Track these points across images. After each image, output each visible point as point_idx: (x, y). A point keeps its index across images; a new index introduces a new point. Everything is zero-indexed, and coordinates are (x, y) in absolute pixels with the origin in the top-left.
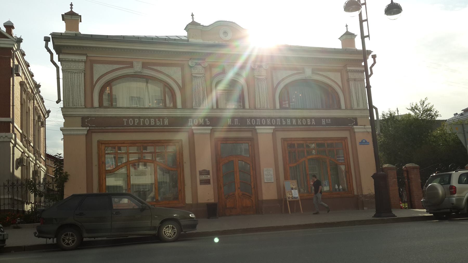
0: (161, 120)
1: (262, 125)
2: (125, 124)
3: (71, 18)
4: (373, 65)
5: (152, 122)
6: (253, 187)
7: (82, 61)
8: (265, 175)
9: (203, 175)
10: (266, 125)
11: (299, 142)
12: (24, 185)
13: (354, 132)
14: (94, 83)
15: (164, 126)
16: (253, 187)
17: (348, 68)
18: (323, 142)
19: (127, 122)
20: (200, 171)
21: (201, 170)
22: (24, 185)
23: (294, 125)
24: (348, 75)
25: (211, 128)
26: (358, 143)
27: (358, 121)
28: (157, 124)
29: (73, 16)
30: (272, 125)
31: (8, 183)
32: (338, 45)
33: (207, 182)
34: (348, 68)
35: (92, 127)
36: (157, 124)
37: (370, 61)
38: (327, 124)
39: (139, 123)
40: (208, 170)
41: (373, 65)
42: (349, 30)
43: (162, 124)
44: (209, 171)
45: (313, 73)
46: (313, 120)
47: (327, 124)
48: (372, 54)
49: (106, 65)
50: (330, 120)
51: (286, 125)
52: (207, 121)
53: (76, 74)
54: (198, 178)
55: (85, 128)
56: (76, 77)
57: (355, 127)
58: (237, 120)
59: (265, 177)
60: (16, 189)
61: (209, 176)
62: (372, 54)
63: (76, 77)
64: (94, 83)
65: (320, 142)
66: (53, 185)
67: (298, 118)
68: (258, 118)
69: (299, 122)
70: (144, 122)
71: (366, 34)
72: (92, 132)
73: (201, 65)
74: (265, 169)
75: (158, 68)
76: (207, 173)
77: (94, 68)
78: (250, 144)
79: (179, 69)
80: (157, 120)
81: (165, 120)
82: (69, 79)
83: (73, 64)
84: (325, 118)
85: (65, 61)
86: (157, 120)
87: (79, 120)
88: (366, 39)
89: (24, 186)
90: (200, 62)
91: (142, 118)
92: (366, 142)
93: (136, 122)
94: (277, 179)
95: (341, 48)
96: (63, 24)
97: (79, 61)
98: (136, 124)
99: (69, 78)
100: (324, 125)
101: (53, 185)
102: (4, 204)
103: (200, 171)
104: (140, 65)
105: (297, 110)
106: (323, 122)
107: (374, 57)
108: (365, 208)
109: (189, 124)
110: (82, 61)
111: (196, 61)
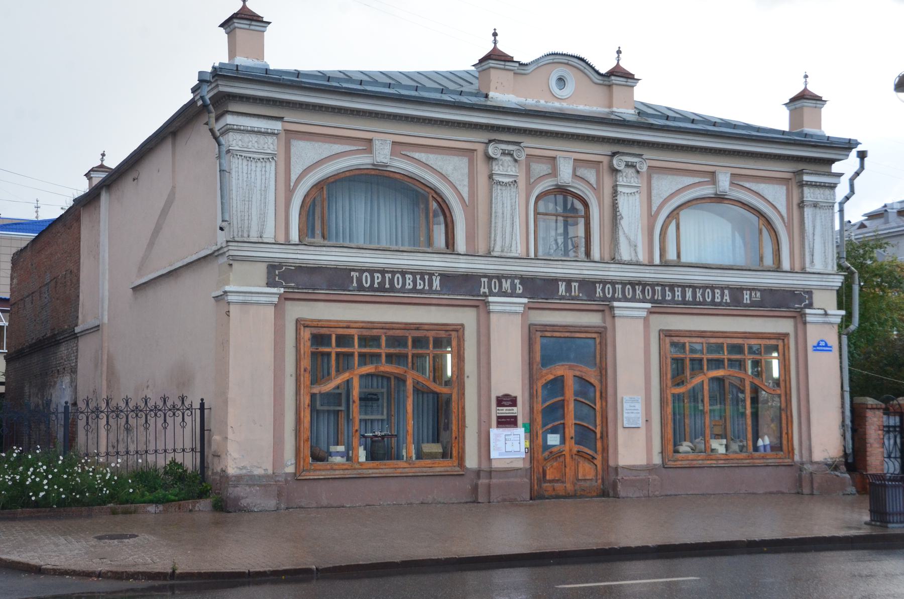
0: (427, 277)
1: (626, 300)
2: (355, 284)
3: (804, 101)
4: (857, 174)
5: (408, 281)
6: (598, 435)
13: (489, 312)
14: (292, 184)
15: (431, 291)
16: (598, 435)
17: (806, 178)
18: (740, 341)
19: (359, 280)
20: (498, 398)
21: (500, 394)
22: (121, 411)
25: (525, 300)
27: (814, 296)
28: (418, 287)
30: (644, 301)
33: (508, 422)
34: (806, 178)
35: (289, 288)
37: (846, 166)
40: (513, 395)
41: (857, 174)
42: (500, 47)
43: (427, 287)
44: (516, 397)
46: (726, 292)
47: (753, 304)
48: (860, 148)
50: (758, 294)
51: (403, 289)
52: (518, 286)
54: (496, 412)
55: (275, 290)
56: (258, 169)
57: (808, 311)
58: (577, 284)
59: (625, 415)
60: (104, 421)
61: (515, 408)
63: (258, 169)
64: (292, 184)
66: (87, 418)
68: (618, 283)
70: (391, 281)
76: (513, 402)
78: (598, 341)
79: (465, 160)
80: (418, 277)
81: (434, 278)
83: (254, 138)
84: (751, 290)
86: (418, 277)
87: (262, 269)
91: (388, 272)
92: (826, 345)
93: (376, 281)
95: (786, 127)
96: (786, 113)
98: (376, 285)
99: (245, 171)
100: (746, 305)
101: (87, 418)
103: (498, 398)
104: (387, 149)
107: (862, 155)
109: (482, 290)
111: (504, 147)
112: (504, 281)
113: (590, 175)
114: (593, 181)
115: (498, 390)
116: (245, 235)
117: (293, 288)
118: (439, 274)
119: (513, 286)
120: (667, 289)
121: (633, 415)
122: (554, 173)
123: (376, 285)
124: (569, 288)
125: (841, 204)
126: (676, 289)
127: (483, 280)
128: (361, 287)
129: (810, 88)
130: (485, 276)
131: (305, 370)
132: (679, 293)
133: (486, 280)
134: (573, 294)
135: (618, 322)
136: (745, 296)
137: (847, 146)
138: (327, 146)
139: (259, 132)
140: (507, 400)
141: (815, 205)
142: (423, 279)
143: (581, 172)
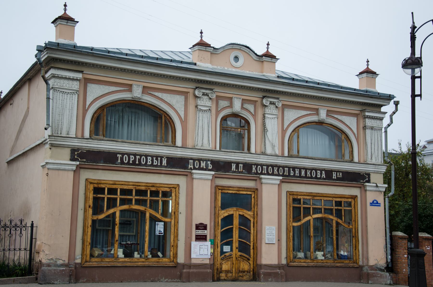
0: (159, 159)
1: (268, 174)
2: (119, 161)
4: (394, 113)
7: (77, 80)
8: (266, 234)
9: (200, 229)
10: (273, 174)
11: (306, 197)
12: (8, 227)
14: (87, 107)
15: (161, 166)
17: (367, 114)
19: (122, 159)
20: (196, 225)
21: (198, 223)
23: (303, 177)
24: (365, 121)
25: (213, 173)
26: (368, 204)
27: (371, 176)
28: (154, 164)
29: (69, 22)
30: (278, 175)
31: (21, 223)
32: (354, 83)
33: (201, 238)
34: (367, 114)
36: (318, 176)
38: (338, 179)
39: (134, 161)
40: (205, 223)
41: (394, 113)
43: (159, 164)
44: (206, 225)
45: (327, 115)
46: (323, 172)
47: (338, 179)
48: (395, 99)
49: (101, 86)
50: (341, 174)
52: (210, 165)
53: (69, 95)
54: (194, 232)
56: (68, 98)
57: (367, 184)
59: (267, 237)
62: (395, 99)
63: (68, 98)
64: (87, 107)
65: (125, 187)
67: (302, 168)
69: (308, 173)
70: (140, 160)
71: (417, 92)
72: (81, 168)
73: (208, 96)
74: (267, 227)
75: (159, 94)
77: (88, 89)
79: (183, 97)
80: (155, 158)
81: (163, 159)
82: (61, 101)
83: (66, 82)
85: (57, 77)
86: (155, 158)
88: (417, 99)
89: (18, 229)
90: (208, 92)
92: (377, 203)
93: (131, 160)
94: (278, 240)
97: (73, 79)
98: (131, 162)
99: (61, 99)
100: (334, 180)
102: (15, 250)
103: (196, 225)
104: (140, 90)
105: (318, 161)
106: (334, 175)
107: (397, 104)
108: (370, 282)
109: (190, 166)
110: (77, 80)
112: (202, 162)
113: (251, 108)
114: (252, 110)
115: (197, 220)
116: (59, 133)
117: (85, 162)
118: (167, 157)
119: (207, 165)
120: (291, 169)
121: (271, 237)
122: (231, 106)
123: (131, 162)
124: (237, 167)
125: (386, 128)
126: (296, 170)
127: (190, 161)
128: (122, 163)
129: (206, 39)
130: (191, 159)
131: (89, 207)
132: (298, 172)
133: (192, 161)
134: (240, 170)
135: (264, 186)
136: (334, 175)
137: (389, 98)
138: (107, 87)
139: (69, 79)
140: (201, 226)
141: (372, 128)
142: (157, 159)
143: (246, 106)
